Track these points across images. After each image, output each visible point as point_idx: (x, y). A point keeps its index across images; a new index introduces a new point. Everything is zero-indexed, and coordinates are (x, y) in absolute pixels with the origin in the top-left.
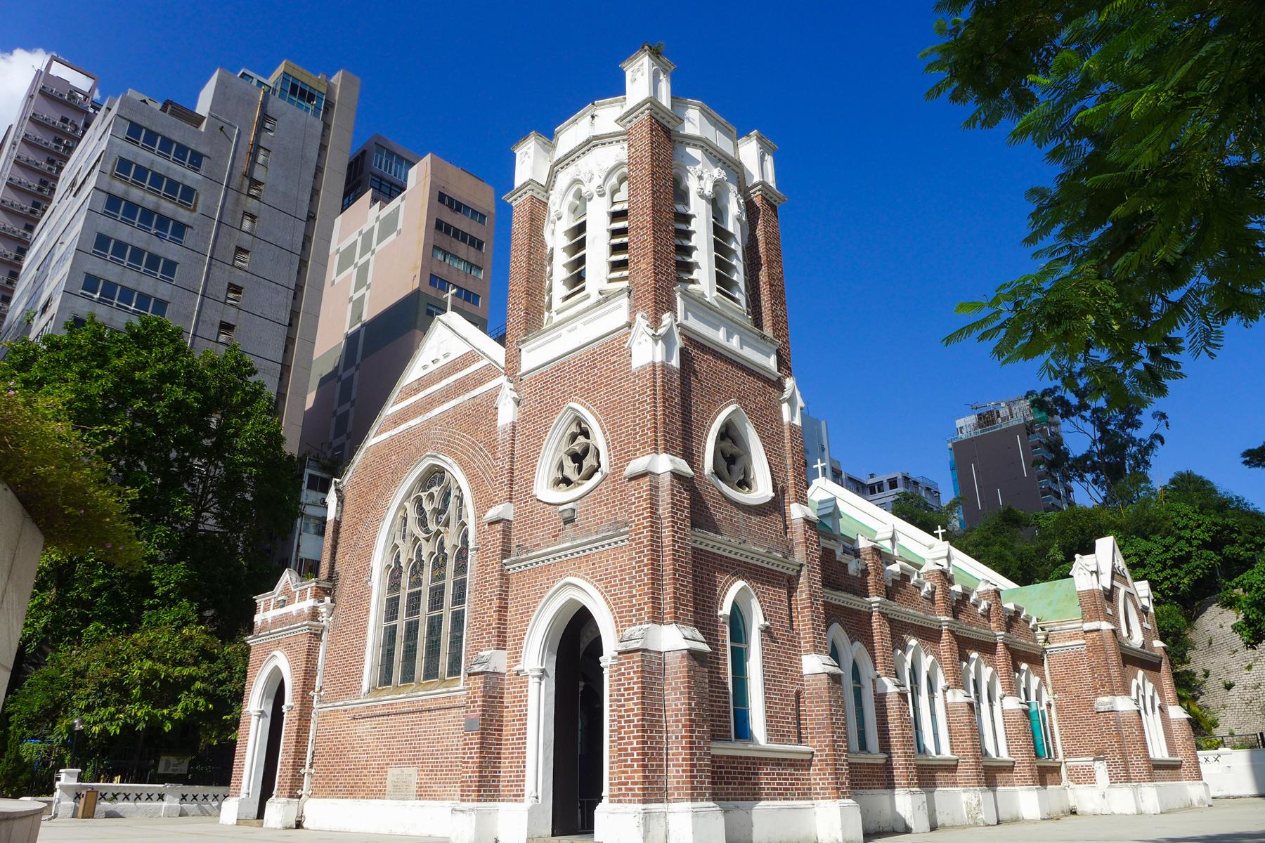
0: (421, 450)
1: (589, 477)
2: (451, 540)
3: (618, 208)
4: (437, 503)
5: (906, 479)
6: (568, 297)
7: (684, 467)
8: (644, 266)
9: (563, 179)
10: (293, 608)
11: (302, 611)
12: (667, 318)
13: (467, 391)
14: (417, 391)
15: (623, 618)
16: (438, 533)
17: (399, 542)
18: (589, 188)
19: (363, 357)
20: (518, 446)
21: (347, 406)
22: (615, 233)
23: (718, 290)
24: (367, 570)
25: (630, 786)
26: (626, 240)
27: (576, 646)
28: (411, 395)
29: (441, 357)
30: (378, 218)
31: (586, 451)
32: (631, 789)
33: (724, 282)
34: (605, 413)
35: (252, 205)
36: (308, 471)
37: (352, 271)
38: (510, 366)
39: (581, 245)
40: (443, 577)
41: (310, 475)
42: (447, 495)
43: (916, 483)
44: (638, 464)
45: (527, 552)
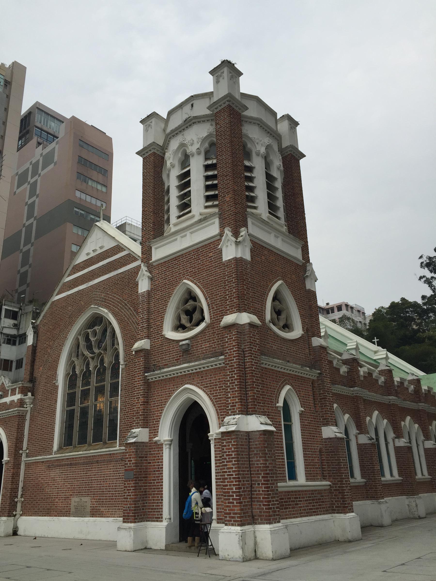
1: (198, 324)
2: (108, 360)
3: (209, 162)
5: (347, 306)
6: (179, 217)
7: (255, 319)
8: (228, 199)
9: (174, 145)
11: (13, 401)
12: (243, 232)
13: (116, 269)
15: (223, 413)
16: (100, 354)
17: (74, 359)
18: (192, 149)
19: (36, 238)
23: (270, 213)
24: (54, 376)
25: (232, 515)
26: (216, 182)
27: (193, 423)
29: (98, 248)
30: (42, 154)
32: (233, 517)
33: (272, 207)
34: (204, 287)
36: (4, 307)
37: (26, 186)
38: (145, 256)
39: (188, 184)
40: (104, 380)
41: (6, 309)
43: (352, 308)
44: (229, 319)
45: (160, 369)
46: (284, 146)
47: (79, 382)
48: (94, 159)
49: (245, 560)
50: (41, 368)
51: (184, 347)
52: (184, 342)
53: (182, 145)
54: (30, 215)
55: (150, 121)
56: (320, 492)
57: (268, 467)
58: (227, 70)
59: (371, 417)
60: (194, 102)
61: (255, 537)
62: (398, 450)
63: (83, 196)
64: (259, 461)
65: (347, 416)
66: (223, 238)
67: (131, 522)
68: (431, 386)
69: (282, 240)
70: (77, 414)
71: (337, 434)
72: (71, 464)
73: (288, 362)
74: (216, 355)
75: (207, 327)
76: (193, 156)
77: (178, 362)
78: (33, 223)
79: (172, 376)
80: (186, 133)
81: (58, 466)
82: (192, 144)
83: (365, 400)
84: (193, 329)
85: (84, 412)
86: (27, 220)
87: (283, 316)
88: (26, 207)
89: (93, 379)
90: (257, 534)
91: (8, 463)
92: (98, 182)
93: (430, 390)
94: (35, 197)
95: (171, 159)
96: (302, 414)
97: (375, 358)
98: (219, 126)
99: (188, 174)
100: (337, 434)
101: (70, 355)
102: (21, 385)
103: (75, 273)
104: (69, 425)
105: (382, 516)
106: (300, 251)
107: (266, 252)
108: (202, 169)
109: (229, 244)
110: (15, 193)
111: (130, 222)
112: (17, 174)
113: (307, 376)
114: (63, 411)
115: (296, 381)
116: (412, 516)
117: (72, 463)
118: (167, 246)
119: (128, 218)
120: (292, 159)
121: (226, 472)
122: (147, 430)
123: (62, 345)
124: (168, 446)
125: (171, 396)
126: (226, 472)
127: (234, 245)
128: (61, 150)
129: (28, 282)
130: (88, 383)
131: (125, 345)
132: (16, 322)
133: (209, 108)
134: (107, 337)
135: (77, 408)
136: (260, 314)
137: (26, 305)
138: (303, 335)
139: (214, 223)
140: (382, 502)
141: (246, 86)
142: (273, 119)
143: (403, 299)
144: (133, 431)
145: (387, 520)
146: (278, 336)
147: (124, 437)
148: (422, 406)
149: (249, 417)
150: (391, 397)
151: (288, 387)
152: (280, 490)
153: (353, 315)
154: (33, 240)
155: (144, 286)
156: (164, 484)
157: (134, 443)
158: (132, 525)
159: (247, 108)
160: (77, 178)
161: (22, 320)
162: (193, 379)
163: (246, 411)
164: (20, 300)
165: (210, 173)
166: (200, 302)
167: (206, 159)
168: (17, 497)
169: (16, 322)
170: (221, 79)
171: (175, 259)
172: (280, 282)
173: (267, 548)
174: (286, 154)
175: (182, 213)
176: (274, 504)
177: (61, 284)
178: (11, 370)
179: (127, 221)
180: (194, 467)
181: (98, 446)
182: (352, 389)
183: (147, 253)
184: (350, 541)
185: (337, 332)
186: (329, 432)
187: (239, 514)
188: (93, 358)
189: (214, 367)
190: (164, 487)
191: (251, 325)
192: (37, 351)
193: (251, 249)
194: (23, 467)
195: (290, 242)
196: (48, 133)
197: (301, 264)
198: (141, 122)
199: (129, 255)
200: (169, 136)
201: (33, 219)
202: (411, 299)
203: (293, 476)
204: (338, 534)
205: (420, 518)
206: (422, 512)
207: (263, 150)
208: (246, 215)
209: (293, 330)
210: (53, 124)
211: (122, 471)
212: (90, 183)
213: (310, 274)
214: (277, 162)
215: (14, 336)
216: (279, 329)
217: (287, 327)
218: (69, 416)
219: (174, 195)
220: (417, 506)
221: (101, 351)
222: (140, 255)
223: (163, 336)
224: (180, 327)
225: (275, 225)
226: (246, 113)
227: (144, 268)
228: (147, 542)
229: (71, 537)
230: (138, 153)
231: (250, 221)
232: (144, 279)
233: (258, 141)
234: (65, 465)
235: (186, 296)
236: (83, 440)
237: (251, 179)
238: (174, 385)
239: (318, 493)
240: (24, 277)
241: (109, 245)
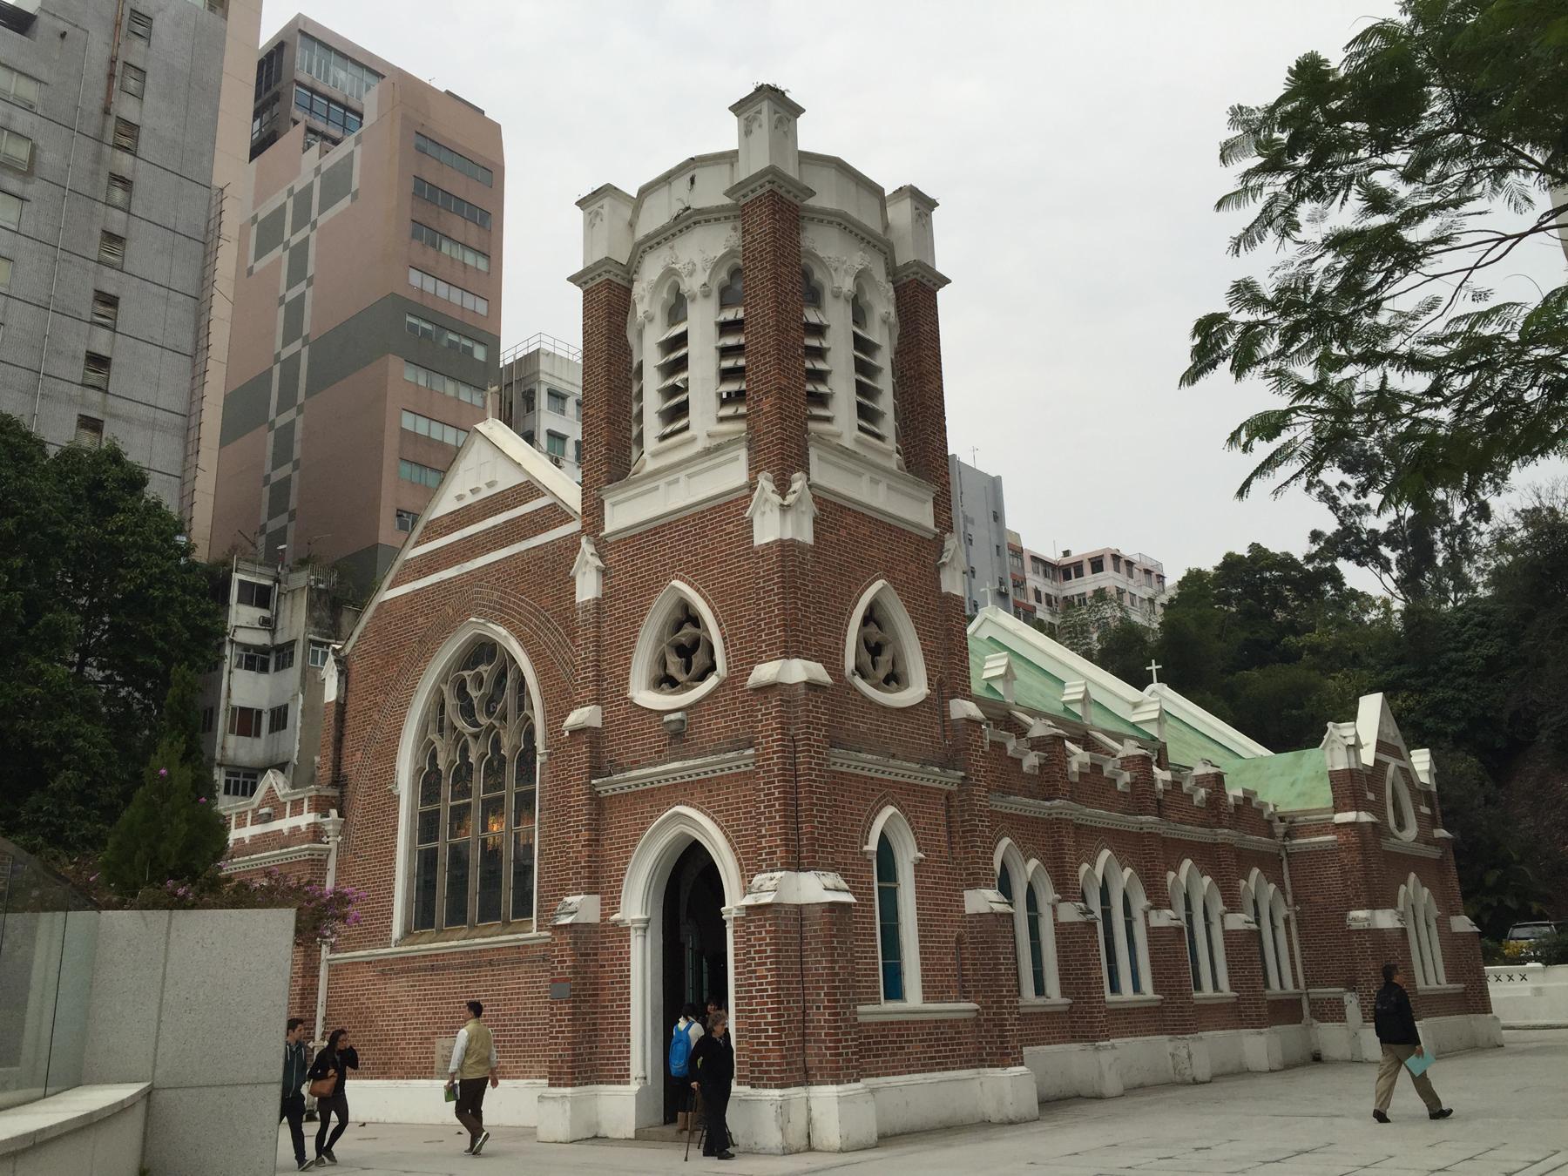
0: (462, 615)
1: (702, 678)
2: (509, 742)
3: (729, 315)
5: (1116, 558)
6: (664, 438)
8: (766, 408)
9: (652, 270)
10: (284, 824)
12: (798, 482)
13: (524, 538)
14: (450, 530)
15: (750, 867)
16: (491, 728)
17: (434, 737)
19: (309, 394)
21: (286, 470)
22: (725, 352)
23: (861, 429)
24: (390, 773)
26: (742, 362)
27: (690, 886)
28: (442, 535)
29: (482, 485)
30: (318, 170)
31: (696, 643)
32: (766, 1072)
34: (718, 600)
35: (124, 163)
39: (681, 364)
40: (501, 786)
41: (241, 582)
42: (502, 675)
43: (1130, 564)
44: (765, 672)
45: (623, 771)
46: (900, 262)
47: (447, 789)
48: (456, 184)
49: (788, 1151)
50: (359, 754)
51: (673, 727)
52: (672, 717)
53: (670, 272)
54: (293, 331)
56: (952, 1024)
57: (837, 974)
58: (770, 107)
59: (1093, 865)
60: (697, 172)
61: (810, 1110)
62: (1154, 934)
63: (429, 284)
64: (819, 962)
65: (1034, 863)
66: (756, 494)
67: (566, 1085)
68: (1250, 788)
69: (889, 487)
70: (444, 859)
71: (995, 906)
72: (433, 968)
73: (893, 756)
74: (738, 745)
75: (721, 685)
76: (693, 300)
79: (649, 786)
80: (679, 242)
81: (403, 971)
82: (691, 274)
83: (1078, 827)
85: (459, 858)
86: (285, 344)
87: (885, 658)
89: (478, 782)
90: (813, 1104)
92: (465, 246)
93: (1248, 797)
95: (646, 300)
96: (919, 866)
97: (1132, 720)
98: (749, 238)
99: (681, 340)
100: (995, 906)
101: (424, 729)
102: (314, 793)
103: (429, 539)
104: (426, 882)
105: (1101, 1076)
106: (929, 508)
107: (849, 520)
108: (713, 331)
109: (767, 508)
110: (250, 271)
111: (551, 349)
112: (255, 218)
113: (936, 785)
114: (410, 852)
115: (908, 797)
116: (1178, 1078)
117: (434, 965)
118: (639, 499)
119: (544, 338)
120: (918, 294)
121: (753, 985)
122: (598, 897)
123: (405, 705)
124: (640, 932)
125: (645, 829)
126: (753, 985)
127: (777, 512)
128: (368, 154)
130: (467, 792)
131: (548, 712)
132: (266, 613)
133: (728, 193)
134: (507, 691)
135: (443, 845)
136: (832, 660)
137: (291, 571)
138: (928, 697)
139: (736, 459)
140: (1105, 1048)
141: (811, 136)
142: (876, 203)
143: (1255, 548)
144: (568, 899)
145: (1112, 1085)
146: (871, 702)
147: (548, 912)
148: (1224, 834)
149: (802, 874)
150: (1143, 818)
151: (889, 810)
152: (861, 1019)
153: (1131, 581)
154: (301, 398)
155: (587, 587)
156: (632, 1008)
157: (571, 925)
158: (568, 1090)
159: (812, 193)
160: (413, 236)
161: (282, 608)
163: (796, 864)
164: (273, 558)
165: (731, 341)
166: (707, 630)
167: (723, 305)
168: (313, 1038)
169: (266, 613)
170: (755, 126)
171: (655, 531)
172: (879, 584)
173: (830, 1131)
174: (905, 280)
175: (668, 430)
176: (849, 1047)
177: (398, 565)
178: (258, 735)
179: (544, 346)
180: (693, 969)
181: (493, 929)
182: (1048, 804)
183: (594, 511)
184: (1011, 1123)
185: (1052, 657)
186: (981, 900)
187: (779, 1065)
188: (476, 736)
189: (735, 770)
190: (632, 1014)
191: (811, 686)
192: (347, 716)
194: (323, 973)
195: (909, 490)
196: (330, 100)
197: (931, 537)
198: (578, 203)
199: (553, 507)
201: (300, 341)
202: (1275, 547)
203: (894, 990)
204: (991, 1109)
205: (1196, 1082)
206: (1202, 1069)
207: (847, 285)
208: (806, 441)
209: (907, 686)
210: (342, 75)
211: (545, 981)
212: (446, 247)
213: (952, 559)
214: (883, 306)
215: (263, 650)
216: (876, 686)
217: (894, 679)
218: (426, 864)
219: (652, 383)
220: (1190, 1057)
222: (579, 510)
223: (629, 701)
224: (664, 681)
225: (871, 456)
226: (811, 202)
227: (587, 547)
228: (598, 1124)
229: (438, 1121)
230: (573, 279)
231: (813, 454)
233: (838, 262)
234: (420, 969)
235: (679, 615)
236: (457, 916)
237: (820, 353)
239: (951, 1027)
240: (280, 492)
241: (507, 480)
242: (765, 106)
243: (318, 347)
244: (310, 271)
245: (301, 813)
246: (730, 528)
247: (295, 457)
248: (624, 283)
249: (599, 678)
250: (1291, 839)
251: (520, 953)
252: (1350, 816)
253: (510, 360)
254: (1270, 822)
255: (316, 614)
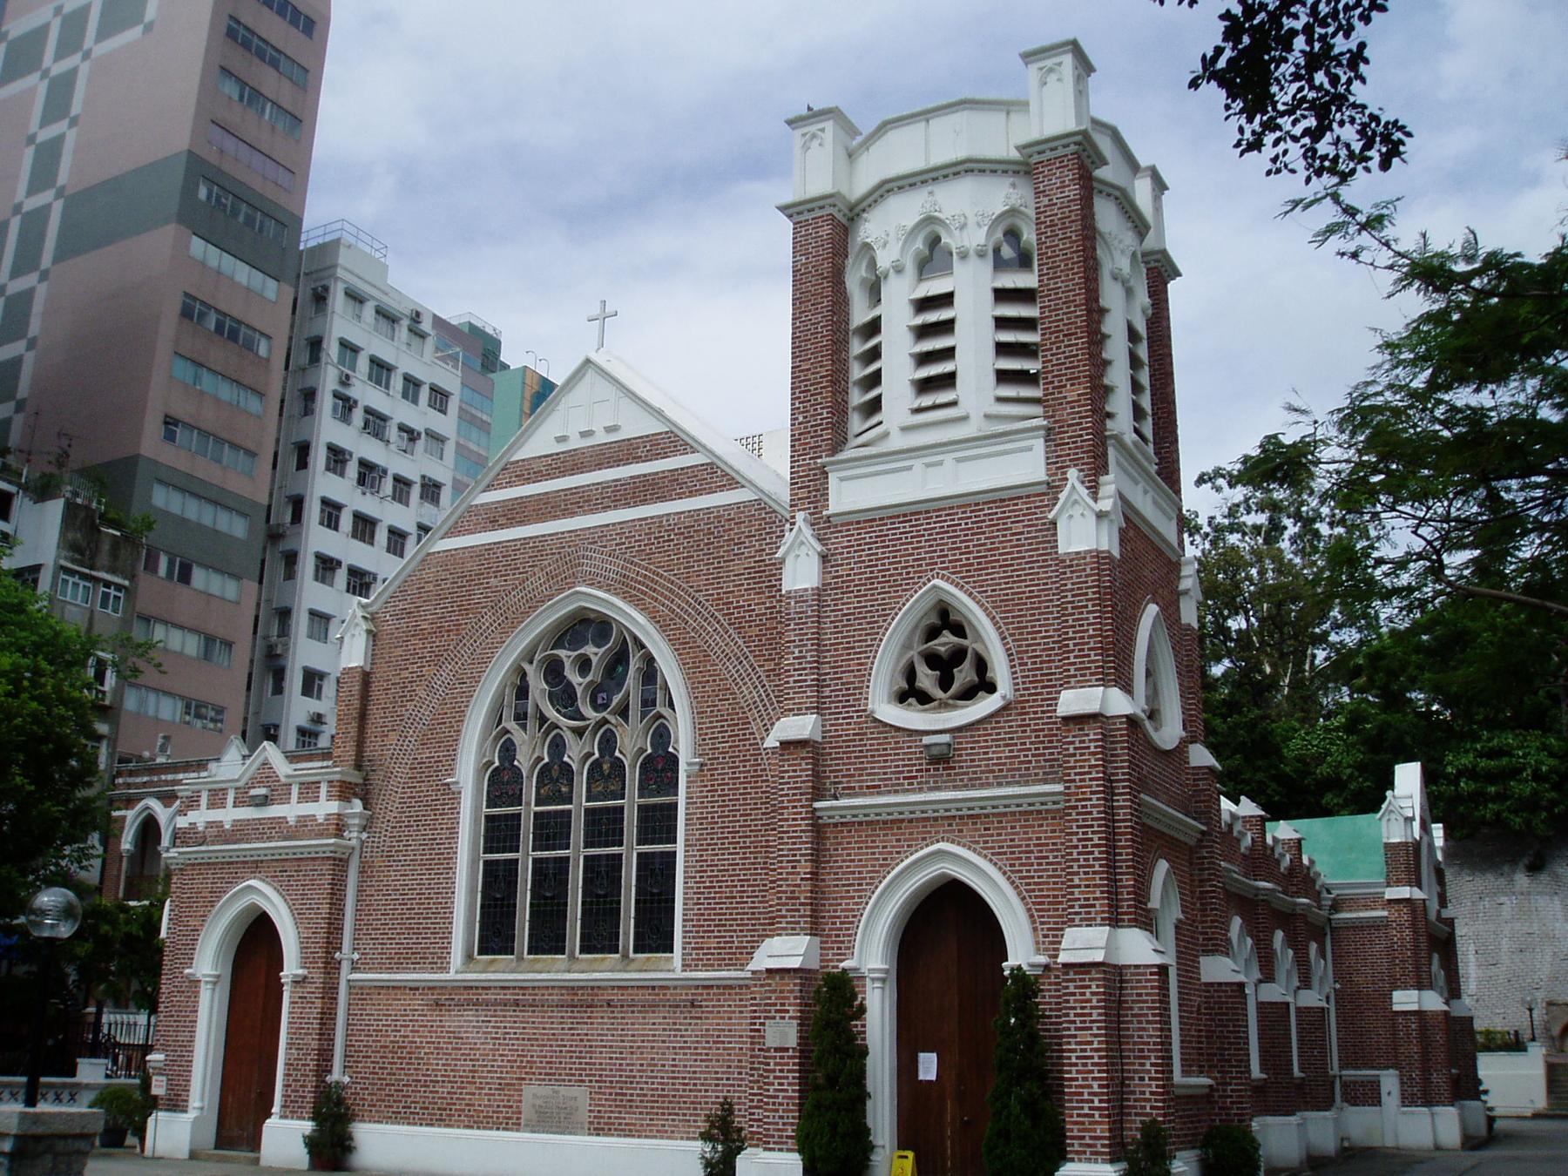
0: (563, 579)
1: (969, 694)
2: (632, 742)
4: (594, 675)
10: (290, 811)
17: (511, 725)
20: (828, 627)
28: (528, 481)
29: (598, 427)
31: (958, 655)
34: (1001, 609)
42: (619, 659)
44: (1072, 701)
50: (393, 736)
51: (935, 751)
54: (43, 176)
55: (820, 126)
77: (911, 781)
78: (49, 206)
81: (469, 1002)
82: (963, 227)
84: (956, 707)
88: (30, 152)
91: (299, 982)
94: (66, 121)
111: (352, 240)
114: (473, 862)
119: (347, 226)
129: (19, 396)
139: (1030, 449)
154: (46, 261)
155: (801, 571)
162: (960, 831)
166: (979, 638)
193: (1121, 531)
200: (887, 186)
221: (609, 717)
224: (910, 693)
232: (803, 555)
234: (496, 1003)
235: (934, 619)
238: (898, 840)
242: (1068, 60)
243: (75, 202)
244: (76, 109)
245: (316, 799)
246: (1019, 528)
247: (30, 335)
248: (844, 221)
249: (819, 685)
250: (1337, 912)
251: (656, 996)
252: (1404, 892)
253: (311, 244)
254: (1319, 893)
255: (70, 535)
